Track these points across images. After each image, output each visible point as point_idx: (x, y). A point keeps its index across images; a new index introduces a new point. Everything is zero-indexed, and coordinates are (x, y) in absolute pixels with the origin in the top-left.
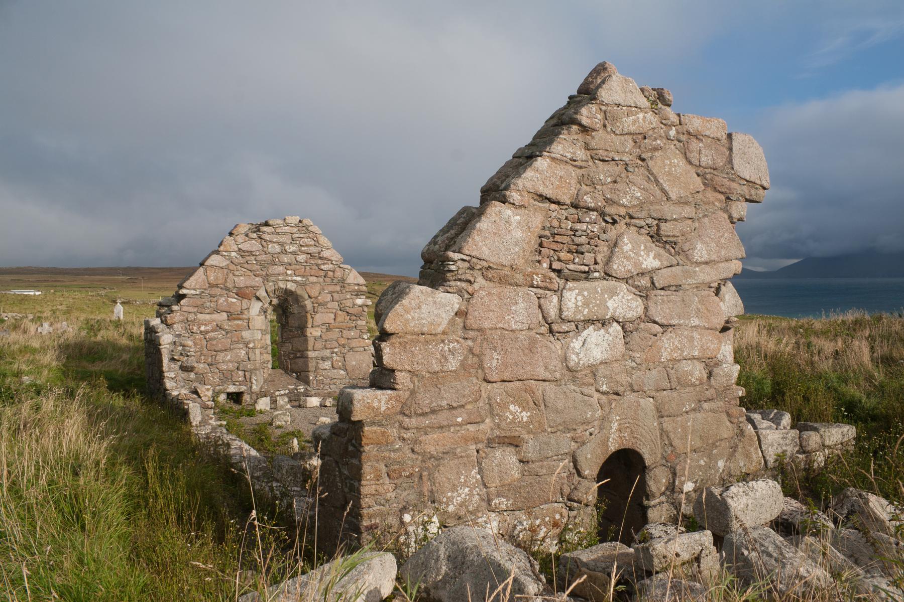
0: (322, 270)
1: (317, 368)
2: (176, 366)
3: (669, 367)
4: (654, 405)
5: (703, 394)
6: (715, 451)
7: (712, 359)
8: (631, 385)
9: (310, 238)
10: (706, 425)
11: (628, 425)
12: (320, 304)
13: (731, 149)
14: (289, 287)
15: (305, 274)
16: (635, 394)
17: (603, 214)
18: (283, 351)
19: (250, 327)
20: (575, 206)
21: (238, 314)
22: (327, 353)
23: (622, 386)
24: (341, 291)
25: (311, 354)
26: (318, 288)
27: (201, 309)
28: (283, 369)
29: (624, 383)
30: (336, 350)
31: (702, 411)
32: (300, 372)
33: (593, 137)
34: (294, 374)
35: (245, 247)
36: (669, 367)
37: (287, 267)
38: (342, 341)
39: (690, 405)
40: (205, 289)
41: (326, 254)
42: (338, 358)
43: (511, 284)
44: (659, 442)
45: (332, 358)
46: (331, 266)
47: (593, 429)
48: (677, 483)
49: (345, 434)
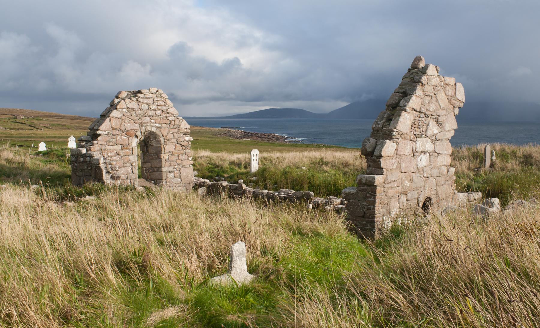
0: (169, 120)
1: (167, 177)
2: (109, 176)
9: (162, 101)
12: (168, 140)
13: (456, 89)
14: (152, 130)
15: (161, 122)
17: (425, 114)
18: (145, 168)
19: (134, 154)
20: (419, 112)
21: (127, 146)
22: (171, 169)
24: (178, 132)
25: (164, 169)
26: (167, 130)
27: (108, 142)
28: (145, 178)
30: (176, 167)
32: (156, 180)
33: (425, 87)
34: (152, 181)
35: (130, 106)
37: (152, 118)
38: (179, 162)
40: (110, 131)
41: (170, 110)
42: (177, 171)
43: (406, 140)
45: (174, 171)
46: (173, 117)
49: (366, 191)
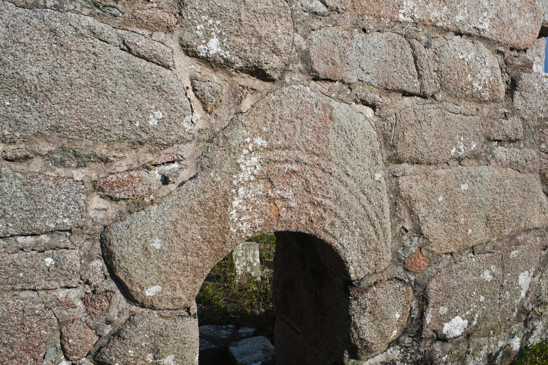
3: (420, 41)
4: (376, 127)
5: (496, 123)
6: (514, 254)
7: (518, 51)
8: (305, 58)
10: (499, 194)
11: (295, 167)
16: (319, 85)
23: (275, 51)
29: (281, 46)
31: (492, 161)
36: (420, 41)
39: (467, 145)
44: (387, 223)
47: (176, 165)
48: (428, 320)
